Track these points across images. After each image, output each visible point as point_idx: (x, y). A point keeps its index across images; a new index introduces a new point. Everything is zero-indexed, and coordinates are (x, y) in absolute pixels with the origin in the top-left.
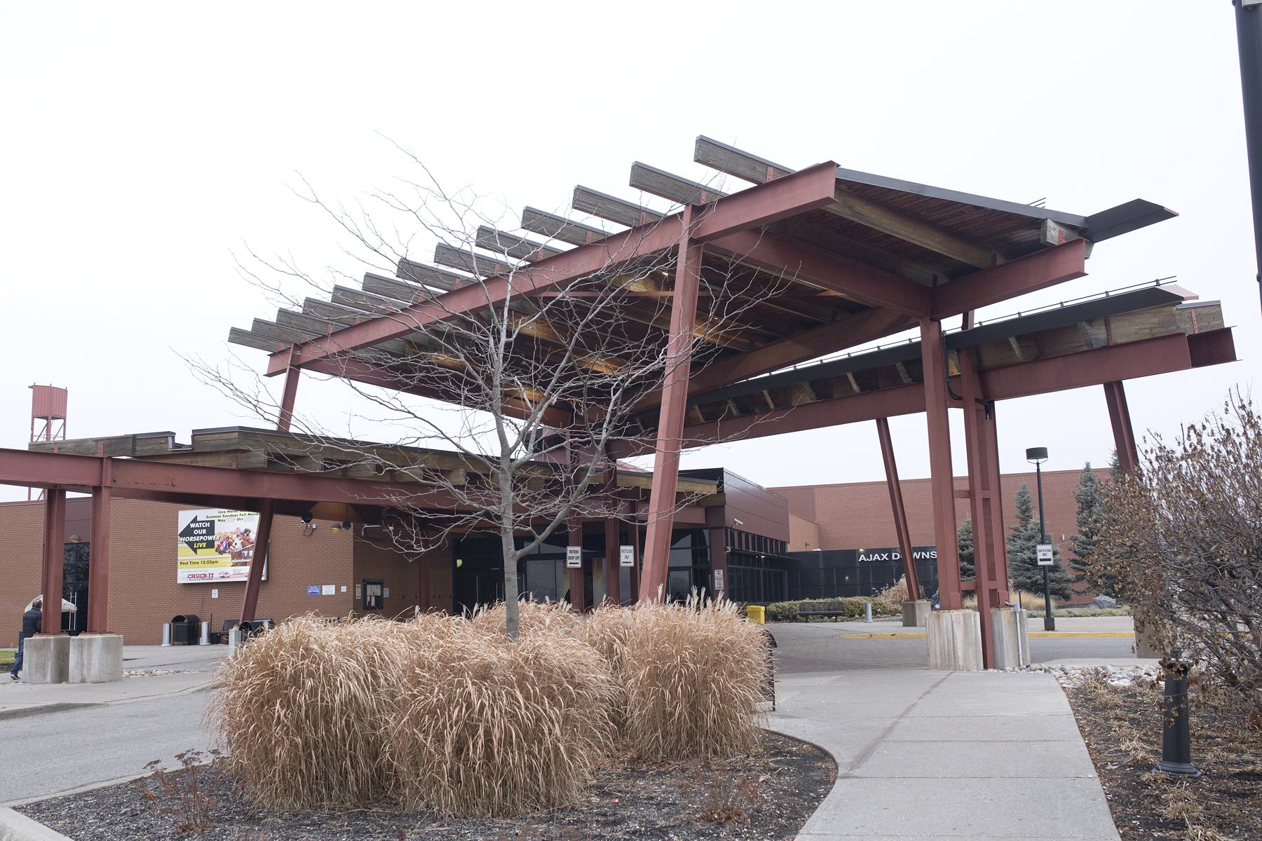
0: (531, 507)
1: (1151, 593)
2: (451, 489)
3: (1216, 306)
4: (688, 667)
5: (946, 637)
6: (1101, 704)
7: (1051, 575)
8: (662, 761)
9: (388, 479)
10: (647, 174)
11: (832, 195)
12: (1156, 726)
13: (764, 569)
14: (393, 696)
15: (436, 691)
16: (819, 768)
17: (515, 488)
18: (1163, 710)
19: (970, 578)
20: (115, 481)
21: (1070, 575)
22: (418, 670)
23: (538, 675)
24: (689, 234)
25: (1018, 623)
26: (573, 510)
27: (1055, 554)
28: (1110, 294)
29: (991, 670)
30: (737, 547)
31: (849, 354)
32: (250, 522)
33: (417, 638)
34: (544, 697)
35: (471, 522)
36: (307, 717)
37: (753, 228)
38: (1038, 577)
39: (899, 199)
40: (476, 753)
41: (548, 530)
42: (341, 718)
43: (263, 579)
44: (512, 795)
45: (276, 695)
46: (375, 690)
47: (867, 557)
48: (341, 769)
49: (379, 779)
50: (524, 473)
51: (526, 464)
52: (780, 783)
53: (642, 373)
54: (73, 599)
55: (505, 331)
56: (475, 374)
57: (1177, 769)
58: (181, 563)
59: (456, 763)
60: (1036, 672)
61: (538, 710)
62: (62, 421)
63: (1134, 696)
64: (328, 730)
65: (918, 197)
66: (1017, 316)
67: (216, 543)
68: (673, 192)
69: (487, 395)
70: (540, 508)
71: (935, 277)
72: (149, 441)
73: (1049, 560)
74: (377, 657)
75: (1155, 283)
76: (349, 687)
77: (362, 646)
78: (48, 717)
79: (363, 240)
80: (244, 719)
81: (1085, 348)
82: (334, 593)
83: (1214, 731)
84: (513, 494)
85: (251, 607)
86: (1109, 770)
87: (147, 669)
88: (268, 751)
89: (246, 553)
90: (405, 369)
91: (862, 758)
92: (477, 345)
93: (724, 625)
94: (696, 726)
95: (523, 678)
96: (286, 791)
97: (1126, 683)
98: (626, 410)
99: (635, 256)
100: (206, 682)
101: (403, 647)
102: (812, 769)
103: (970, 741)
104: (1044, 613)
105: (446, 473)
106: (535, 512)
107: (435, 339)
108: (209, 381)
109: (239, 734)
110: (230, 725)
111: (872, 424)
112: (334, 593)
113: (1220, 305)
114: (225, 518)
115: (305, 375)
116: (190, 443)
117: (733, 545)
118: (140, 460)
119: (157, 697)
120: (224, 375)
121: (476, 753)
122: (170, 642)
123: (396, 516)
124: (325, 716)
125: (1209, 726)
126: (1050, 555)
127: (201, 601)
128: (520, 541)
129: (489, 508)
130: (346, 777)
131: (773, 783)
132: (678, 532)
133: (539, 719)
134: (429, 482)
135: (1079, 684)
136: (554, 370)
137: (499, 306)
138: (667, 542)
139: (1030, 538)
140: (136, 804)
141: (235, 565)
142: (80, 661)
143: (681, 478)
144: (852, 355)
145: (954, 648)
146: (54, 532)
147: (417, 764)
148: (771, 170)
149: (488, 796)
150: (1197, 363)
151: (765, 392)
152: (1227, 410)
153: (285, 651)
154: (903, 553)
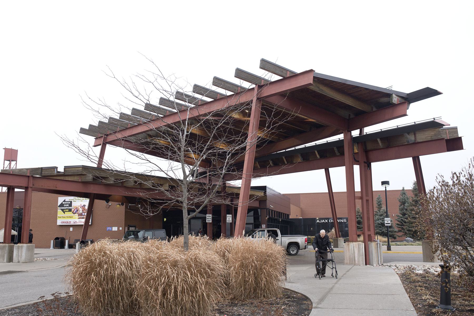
0: (195, 199)
1: (440, 238)
2: (164, 191)
3: (456, 129)
4: (254, 263)
5: (351, 252)
6: (413, 280)
7: (389, 229)
8: (243, 300)
9: (139, 187)
10: (241, 73)
11: (312, 82)
12: (435, 289)
13: (281, 225)
14: (138, 273)
15: (156, 271)
16: (305, 304)
17: (188, 191)
18: (444, 285)
19: (358, 230)
20: (34, 185)
21: (396, 229)
22: (149, 262)
23: (196, 265)
24: (257, 96)
25: (379, 248)
26: (211, 200)
27: (391, 221)
28: (416, 123)
29: (368, 266)
30: (271, 216)
31: (316, 144)
32: (85, 202)
33: (149, 249)
34: (198, 274)
35: (171, 204)
36: (104, 280)
37: (282, 94)
38: (384, 230)
39: (337, 85)
40: (171, 296)
41: (201, 208)
42: (118, 280)
43: (90, 224)
44: (185, 313)
45: (92, 271)
46: (131, 270)
47: (320, 221)
48: (117, 301)
49: (132, 305)
50: (192, 185)
51: (192, 182)
52: (290, 310)
53: (238, 148)
54: (17, 230)
55: (186, 130)
56: (174, 146)
57: (446, 308)
58: (59, 217)
59: (163, 300)
60: (385, 267)
61: (195, 279)
62: (15, 162)
63: (425, 277)
64: (112, 285)
65: (344, 84)
66: (380, 131)
67: (72, 210)
68: (251, 80)
69: (178, 155)
70: (198, 199)
71: (350, 115)
72: (47, 170)
73: (389, 224)
74: (132, 257)
75: (433, 119)
76: (121, 268)
77: (127, 252)
78: (4, 276)
79: (132, 93)
80: (79, 280)
81: (406, 143)
82: (117, 230)
83: (457, 292)
84: (187, 193)
85: (85, 235)
86: (419, 307)
87: (44, 258)
88: (88, 293)
89: (84, 214)
90: (147, 144)
91: (321, 300)
92: (175, 136)
93: (269, 246)
94: (257, 286)
95: (190, 267)
96: (95, 309)
97: (421, 272)
98: (232, 162)
99: (252, 84)
100: (66, 264)
101: (143, 253)
102: (302, 304)
103: (363, 294)
104: (387, 244)
105: (162, 185)
106: (196, 200)
107: (158, 133)
108: (69, 146)
109: (77, 286)
110: (74, 282)
111: (323, 171)
112: (117, 230)
113: (457, 128)
114: (76, 200)
115: (108, 147)
116: (63, 171)
117: (269, 215)
118: (45, 177)
119: (47, 269)
120: (76, 143)
121: (171, 296)
122: (53, 247)
123: (142, 201)
124: (111, 279)
125: (455, 290)
126: (389, 222)
127: (66, 232)
128: (190, 211)
129: (178, 199)
130: (119, 304)
131: (287, 309)
132: (249, 210)
133: (196, 283)
134: (155, 188)
135: (403, 272)
136: (205, 146)
137: (184, 121)
138: (246, 213)
139: (381, 215)
140: (35, 313)
141: (79, 218)
142: (18, 254)
143: (252, 190)
144: (317, 144)
145: (354, 257)
146: (9, 204)
147: (147, 299)
148: (288, 72)
149: (175, 313)
150: (449, 150)
151: (284, 157)
152: (470, 167)
153: (96, 253)
154: (334, 219)
